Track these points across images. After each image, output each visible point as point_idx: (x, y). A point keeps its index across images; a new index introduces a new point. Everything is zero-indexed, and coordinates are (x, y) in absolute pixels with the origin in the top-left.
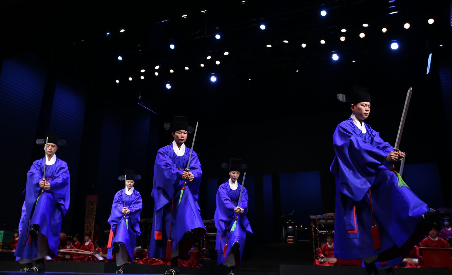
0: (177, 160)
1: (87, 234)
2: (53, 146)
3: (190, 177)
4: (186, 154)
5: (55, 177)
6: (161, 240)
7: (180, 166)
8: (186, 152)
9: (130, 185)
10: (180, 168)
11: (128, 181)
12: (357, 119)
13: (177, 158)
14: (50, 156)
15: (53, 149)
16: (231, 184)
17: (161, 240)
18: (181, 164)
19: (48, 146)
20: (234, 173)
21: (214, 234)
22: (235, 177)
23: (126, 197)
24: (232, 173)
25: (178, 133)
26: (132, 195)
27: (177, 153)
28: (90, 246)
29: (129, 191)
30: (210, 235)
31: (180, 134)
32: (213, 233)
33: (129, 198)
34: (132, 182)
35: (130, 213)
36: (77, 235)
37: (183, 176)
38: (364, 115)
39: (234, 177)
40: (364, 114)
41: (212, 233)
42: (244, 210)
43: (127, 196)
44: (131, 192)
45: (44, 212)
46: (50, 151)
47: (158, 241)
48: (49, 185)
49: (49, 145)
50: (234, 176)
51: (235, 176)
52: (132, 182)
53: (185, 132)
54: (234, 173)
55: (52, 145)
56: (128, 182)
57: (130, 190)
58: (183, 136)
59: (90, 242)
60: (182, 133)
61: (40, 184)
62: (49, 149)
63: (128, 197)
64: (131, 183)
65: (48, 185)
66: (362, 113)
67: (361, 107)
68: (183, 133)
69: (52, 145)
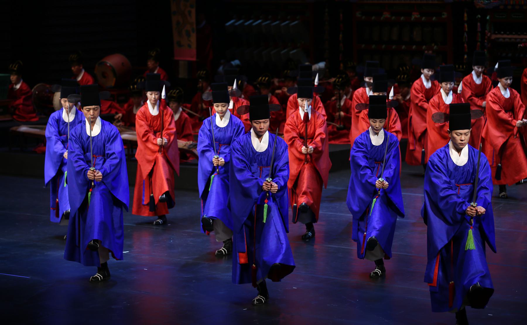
0: (257, 157)
1: (173, 97)
2: (96, 109)
3: (272, 189)
4: (270, 148)
5: (108, 154)
6: (247, 263)
7: (263, 165)
8: (270, 144)
9: (221, 111)
10: (263, 168)
11: (217, 106)
12: (455, 149)
13: (258, 156)
14: (92, 123)
15: (96, 113)
16: (373, 135)
17: (247, 263)
18: (264, 163)
19: (89, 111)
20: (374, 121)
21: (510, 39)
22: (376, 127)
23: (219, 131)
24: (372, 121)
25: (255, 122)
26: (228, 126)
27: (257, 148)
28: (182, 123)
29: (221, 120)
30: (501, 40)
31: (259, 125)
32: (508, 35)
33: (224, 132)
34: (223, 105)
35: (225, 164)
36: (153, 54)
37: (264, 188)
38: (459, 145)
39: (375, 128)
40: (459, 144)
41: (505, 36)
42: (389, 184)
43: (220, 129)
44: (225, 121)
45: (103, 219)
46: (92, 117)
47: (242, 265)
48: (101, 176)
49: (90, 109)
50: (376, 126)
51: (377, 126)
52: (224, 107)
53: (265, 121)
54: (374, 121)
55: (94, 109)
56: (217, 107)
57: (223, 119)
58: (262, 127)
59: (181, 114)
60: (260, 123)
61: (88, 175)
62: (91, 115)
63: (221, 131)
64: (222, 109)
65: (99, 176)
66: (458, 144)
67: (455, 135)
68: (262, 124)
69: (94, 109)
